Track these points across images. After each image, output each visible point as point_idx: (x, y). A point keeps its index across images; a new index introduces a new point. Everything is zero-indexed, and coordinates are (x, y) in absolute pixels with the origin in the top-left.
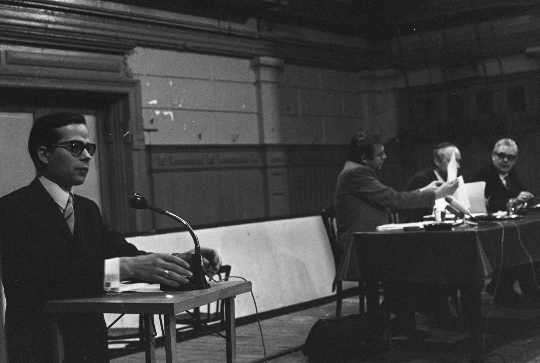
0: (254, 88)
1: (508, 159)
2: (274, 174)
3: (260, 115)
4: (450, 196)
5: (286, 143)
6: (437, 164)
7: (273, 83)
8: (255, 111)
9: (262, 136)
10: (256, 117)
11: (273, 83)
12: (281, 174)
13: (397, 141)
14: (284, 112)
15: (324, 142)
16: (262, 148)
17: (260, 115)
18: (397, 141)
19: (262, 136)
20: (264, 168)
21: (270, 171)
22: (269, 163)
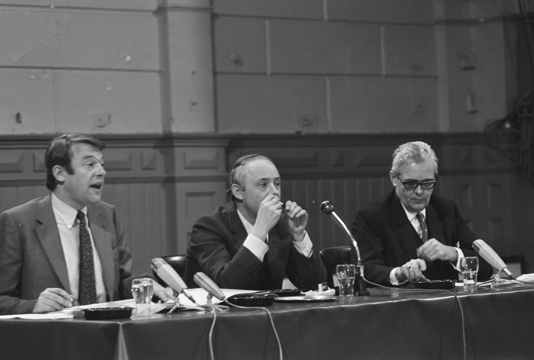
0: (154, 20)
1: (423, 189)
2: (189, 195)
3: (164, 73)
4: (305, 223)
5: (222, 131)
6: (239, 196)
7: (159, 72)
8: (157, 67)
9: (168, 119)
10: (156, 78)
11: (159, 72)
12: (211, 194)
13: (508, 126)
14: (220, 72)
15: (328, 126)
16: (166, 142)
17: (164, 73)
18: (508, 126)
19: (168, 119)
20: (169, 181)
21: (181, 188)
22: (179, 172)
